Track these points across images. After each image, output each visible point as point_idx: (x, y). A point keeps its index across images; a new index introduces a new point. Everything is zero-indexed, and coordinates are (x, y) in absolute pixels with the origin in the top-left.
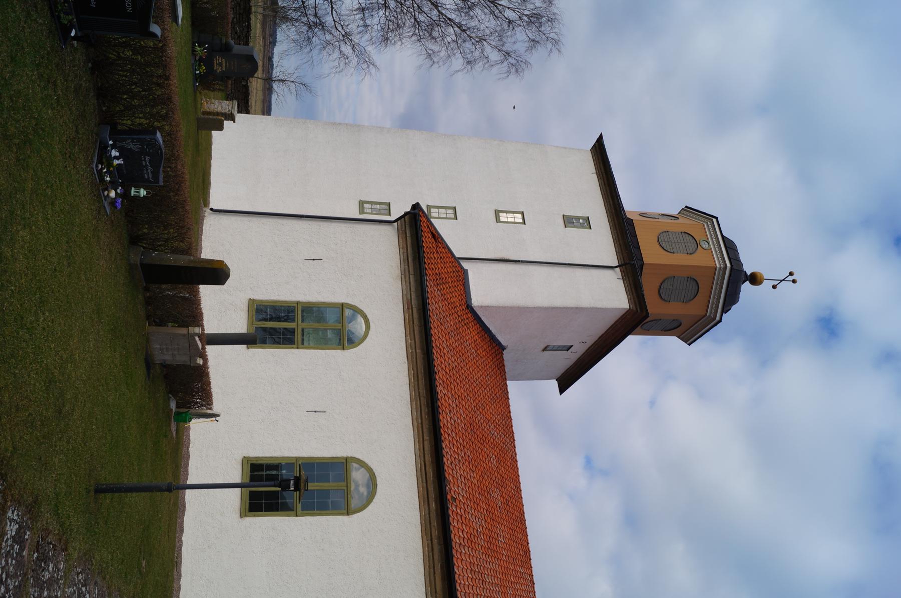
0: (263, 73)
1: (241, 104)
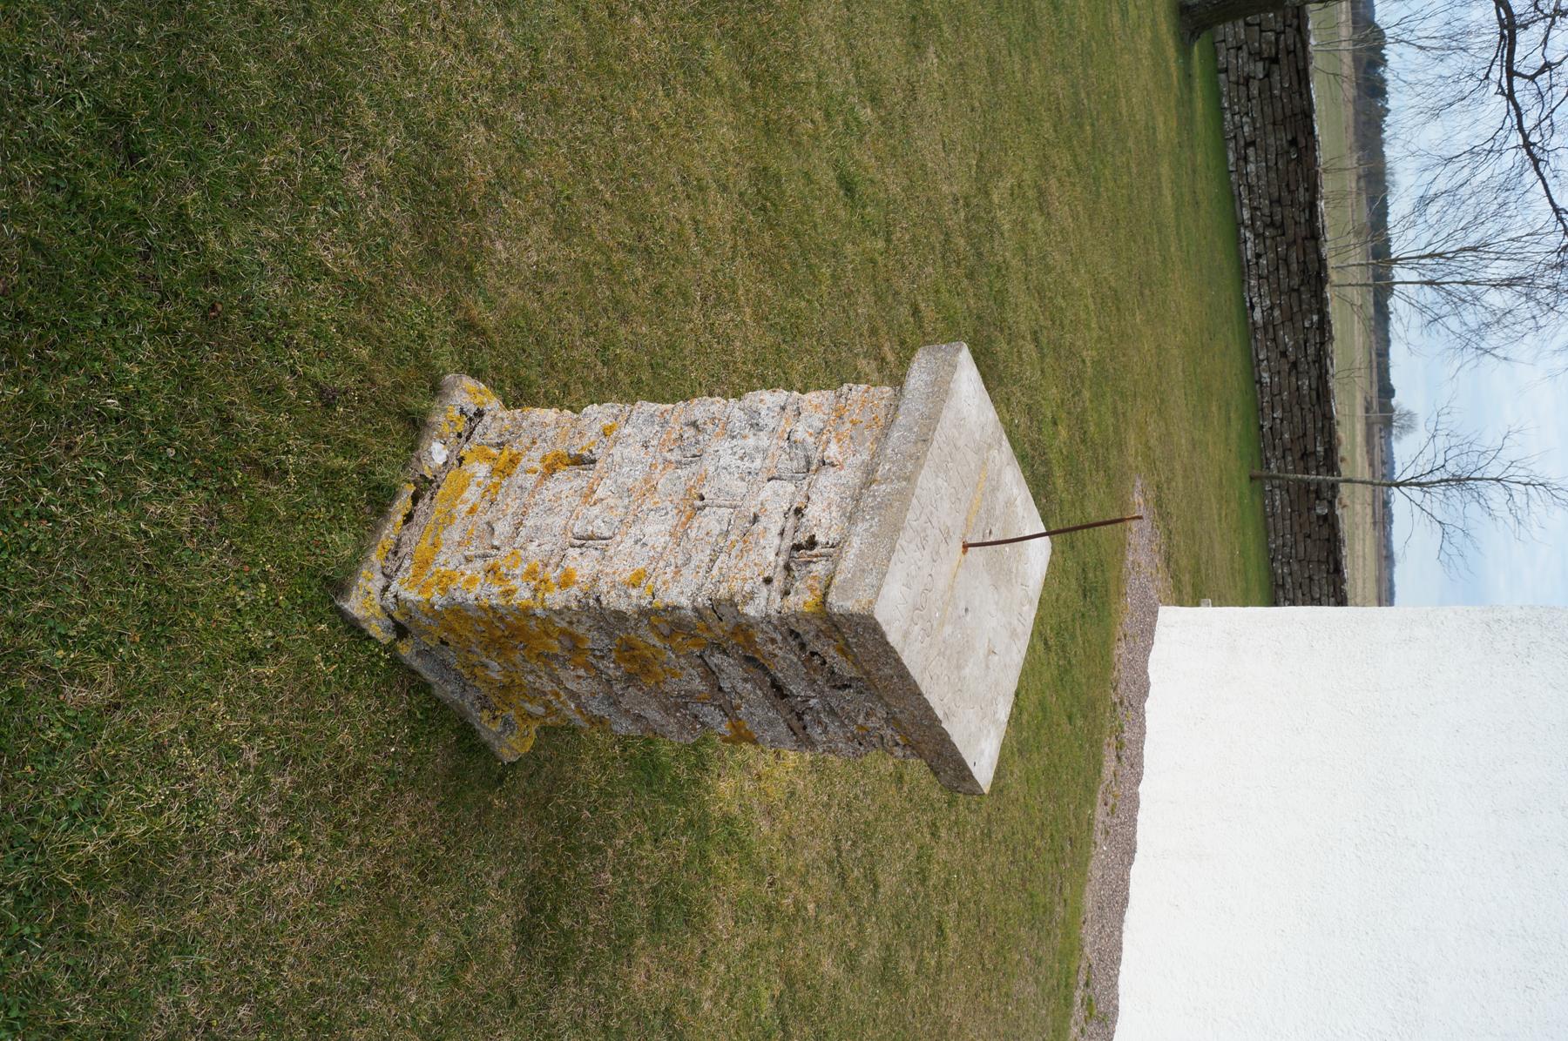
0: (1374, 529)
1: (1316, 578)
